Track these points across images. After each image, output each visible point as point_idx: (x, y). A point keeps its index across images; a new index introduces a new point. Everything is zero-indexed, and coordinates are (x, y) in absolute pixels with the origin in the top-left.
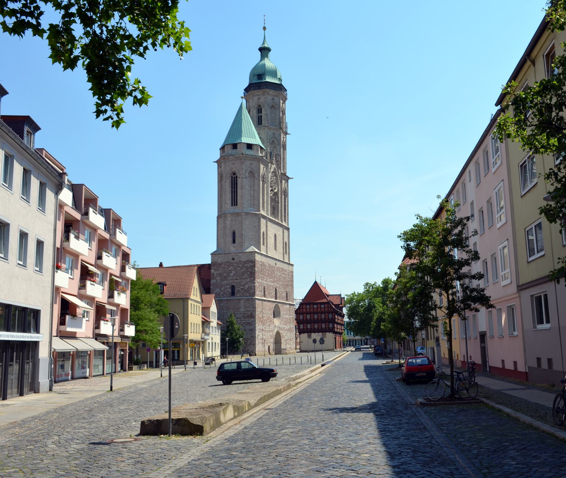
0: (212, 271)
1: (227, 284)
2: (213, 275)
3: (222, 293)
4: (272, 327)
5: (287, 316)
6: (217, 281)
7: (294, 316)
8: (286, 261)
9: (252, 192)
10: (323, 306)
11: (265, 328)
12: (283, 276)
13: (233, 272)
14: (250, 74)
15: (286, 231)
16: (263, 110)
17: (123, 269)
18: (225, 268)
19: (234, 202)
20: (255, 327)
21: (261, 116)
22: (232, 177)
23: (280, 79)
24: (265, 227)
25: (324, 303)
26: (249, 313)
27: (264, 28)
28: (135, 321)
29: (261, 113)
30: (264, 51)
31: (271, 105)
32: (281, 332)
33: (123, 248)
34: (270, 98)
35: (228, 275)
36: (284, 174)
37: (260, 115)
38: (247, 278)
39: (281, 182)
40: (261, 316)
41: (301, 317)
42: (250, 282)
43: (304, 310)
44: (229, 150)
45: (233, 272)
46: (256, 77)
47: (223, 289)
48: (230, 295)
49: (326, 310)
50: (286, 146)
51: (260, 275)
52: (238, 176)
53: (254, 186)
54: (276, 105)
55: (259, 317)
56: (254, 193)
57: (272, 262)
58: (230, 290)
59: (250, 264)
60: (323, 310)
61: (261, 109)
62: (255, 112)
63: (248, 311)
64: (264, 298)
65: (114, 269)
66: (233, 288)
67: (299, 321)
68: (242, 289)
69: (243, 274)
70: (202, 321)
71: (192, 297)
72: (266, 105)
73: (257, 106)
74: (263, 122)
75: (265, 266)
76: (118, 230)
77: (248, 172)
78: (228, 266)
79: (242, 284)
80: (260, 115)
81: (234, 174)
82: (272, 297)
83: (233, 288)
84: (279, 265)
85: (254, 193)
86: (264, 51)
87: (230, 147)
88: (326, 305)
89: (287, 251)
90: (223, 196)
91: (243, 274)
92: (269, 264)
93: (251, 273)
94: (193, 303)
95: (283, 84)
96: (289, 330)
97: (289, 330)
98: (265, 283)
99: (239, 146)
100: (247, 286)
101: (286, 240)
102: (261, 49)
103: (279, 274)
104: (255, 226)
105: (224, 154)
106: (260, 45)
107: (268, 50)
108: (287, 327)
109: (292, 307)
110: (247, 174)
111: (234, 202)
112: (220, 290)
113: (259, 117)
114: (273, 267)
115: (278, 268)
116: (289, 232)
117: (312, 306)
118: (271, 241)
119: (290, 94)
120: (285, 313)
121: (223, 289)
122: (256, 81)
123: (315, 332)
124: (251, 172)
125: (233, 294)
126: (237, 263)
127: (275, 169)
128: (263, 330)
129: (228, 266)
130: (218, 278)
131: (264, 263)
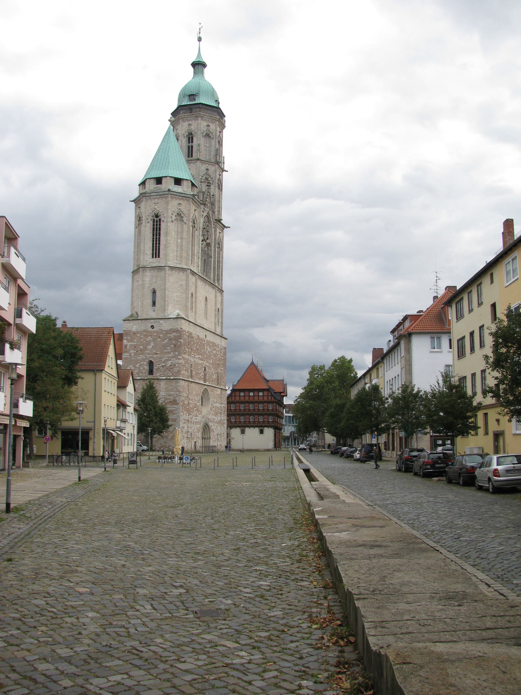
0: (125, 342)
1: (143, 360)
2: (126, 347)
3: (136, 371)
4: (199, 418)
5: (218, 405)
6: (130, 355)
7: (225, 405)
8: (218, 332)
9: (179, 241)
10: (261, 394)
11: (191, 418)
12: (214, 352)
13: (152, 344)
14: (180, 95)
15: (219, 294)
16: (195, 139)
17: (19, 314)
18: (141, 338)
19: (156, 253)
20: (179, 416)
21: (192, 147)
22: (154, 220)
23: (217, 101)
24: (194, 286)
25: (262, 390)
26: (172, 398)
27: (200, 39)
28: (32, 393)
29: (192, 142)
30: (198, 66)
31: (205, 134)
32: (210, 424)
33: (19, 281)
34: (205, 124)
35: (145, 348)
36: (219, 221)
37: (190, 144)
38: (169, 353)
39: (215, 231)
40: (186, 402)
41: (233, 407)
42: (173, 357)
43: (237, 398)
44: (151, 186)
45: (152, 344)
46: (187, 98)
47: (137, 366)
48: (147, 373)
49: (266, 398)
50: (222, 184)
51: (187, 349)
52: (162, 219)
53: (182, 232)
54: (212, 133)
55: (184, 404)
56: (182, 242)
57: (201, 334)
58: (147, 368)
59: (174, 334)
60: (261, 398)
61: (192, 138)
62: (184, 141)
63: (170, 395)
64: (190, 380)
65: (7, 309)
66: (151, 363)
67: (229, 415)
68: (163, 366)
69: (165, 346)
70: (118, 405)
71: (107, 369)
72: (199, 133)
73: (187, 134)
74: (194, 154)
75: (192, 337)
76: (13, 250)
77: (176, 214)
78: (145, 335)
79: (163, 360)
80: (190, 144)
81: (157, 216)
82: (200, 379)
83: (151, 363)
84: (211, 338)
85: (182, 242)
86: (198, 66)
87: (153, 182)
88: (266, 393)
89: (220, 320)
90: (142, 245)
91: (165, 346)
92: (198, 336)
93: (175, 346)
94: (107, 378)
95: (220, 106)
96: (220, 422)
97: (220, 422)
98: (193, 360)
99: (164, 180)
100: (169, 363)
101: (219, 306)
102: (194, 65)
103: (209, 349)
104: (181, 285)
105: (144, 191)
106: (193, 59)
107: (204, 65)
108: (217, 419)
109: (224, 392)
110: (174, 218)
111: (156, 253)
112: (135, 366)
113: (189, 147)
114: (203, 340)
115: (208, 342)
116: (222, 296)
117: (247, 393)
118: (201, 305)
119: (228, 120)
120: (215, 401)
121: (137, 366)
122: (186, 102)
123: (250, 427)
124: (179, 215)
125: (151, 372)
126: (157, 332)
127: (208, 213)
128: (188, 421)
129: (145, 335)
130: (132, 351)
131: (191, 334)
